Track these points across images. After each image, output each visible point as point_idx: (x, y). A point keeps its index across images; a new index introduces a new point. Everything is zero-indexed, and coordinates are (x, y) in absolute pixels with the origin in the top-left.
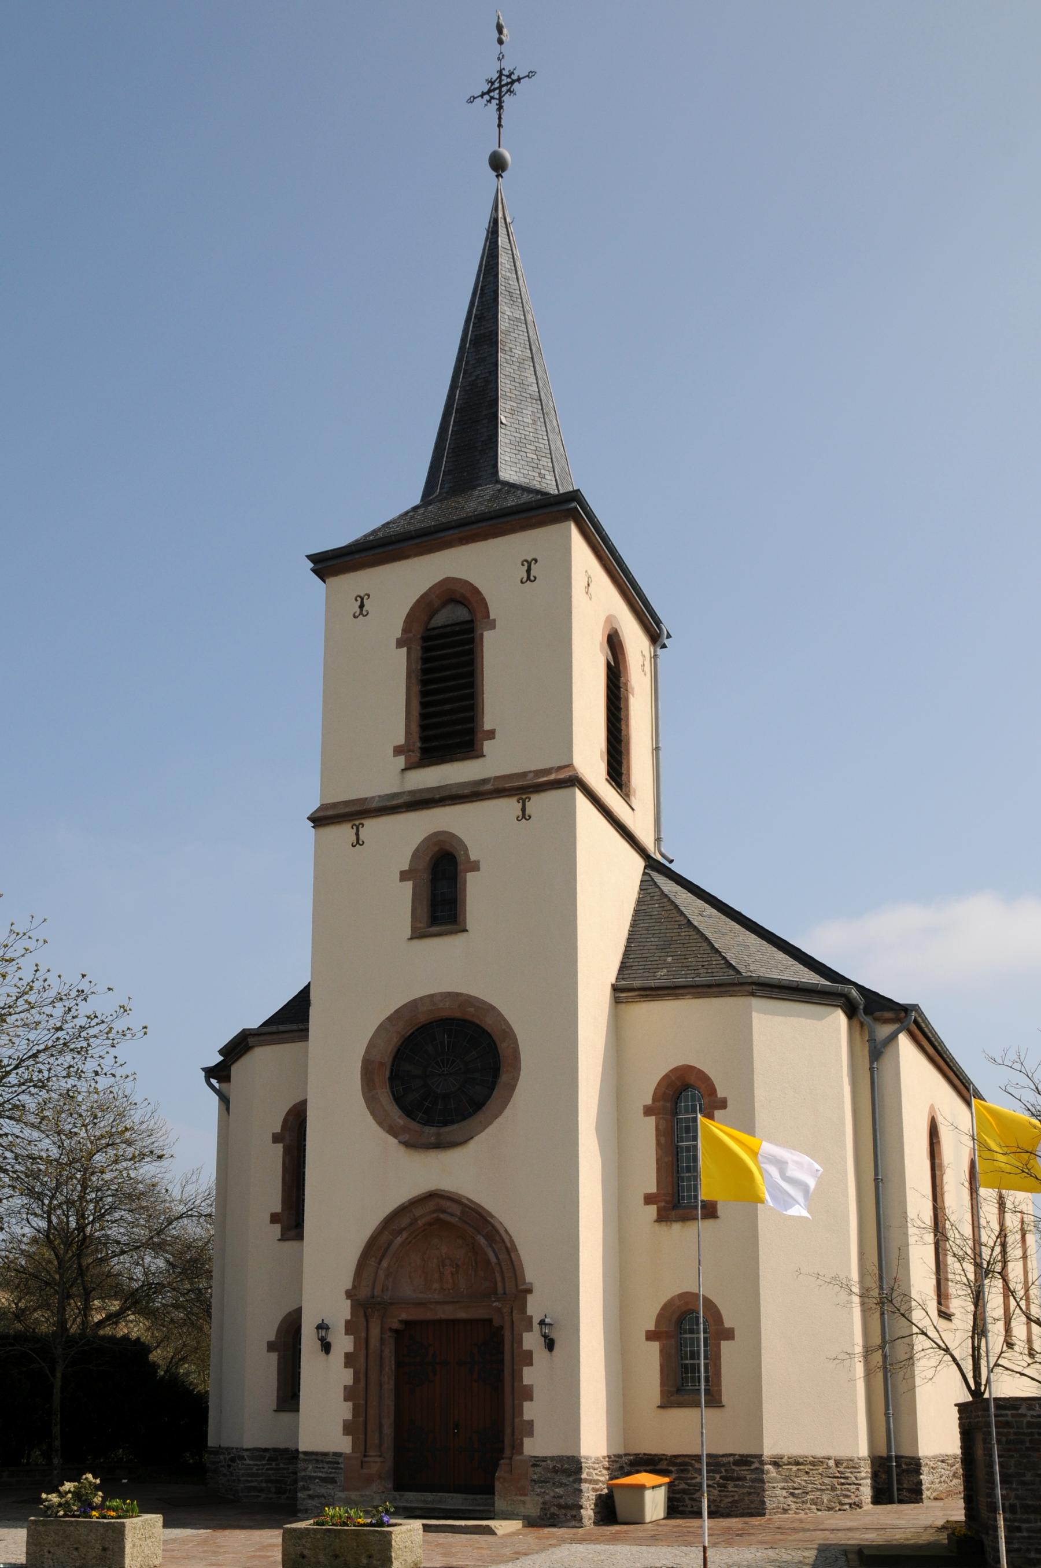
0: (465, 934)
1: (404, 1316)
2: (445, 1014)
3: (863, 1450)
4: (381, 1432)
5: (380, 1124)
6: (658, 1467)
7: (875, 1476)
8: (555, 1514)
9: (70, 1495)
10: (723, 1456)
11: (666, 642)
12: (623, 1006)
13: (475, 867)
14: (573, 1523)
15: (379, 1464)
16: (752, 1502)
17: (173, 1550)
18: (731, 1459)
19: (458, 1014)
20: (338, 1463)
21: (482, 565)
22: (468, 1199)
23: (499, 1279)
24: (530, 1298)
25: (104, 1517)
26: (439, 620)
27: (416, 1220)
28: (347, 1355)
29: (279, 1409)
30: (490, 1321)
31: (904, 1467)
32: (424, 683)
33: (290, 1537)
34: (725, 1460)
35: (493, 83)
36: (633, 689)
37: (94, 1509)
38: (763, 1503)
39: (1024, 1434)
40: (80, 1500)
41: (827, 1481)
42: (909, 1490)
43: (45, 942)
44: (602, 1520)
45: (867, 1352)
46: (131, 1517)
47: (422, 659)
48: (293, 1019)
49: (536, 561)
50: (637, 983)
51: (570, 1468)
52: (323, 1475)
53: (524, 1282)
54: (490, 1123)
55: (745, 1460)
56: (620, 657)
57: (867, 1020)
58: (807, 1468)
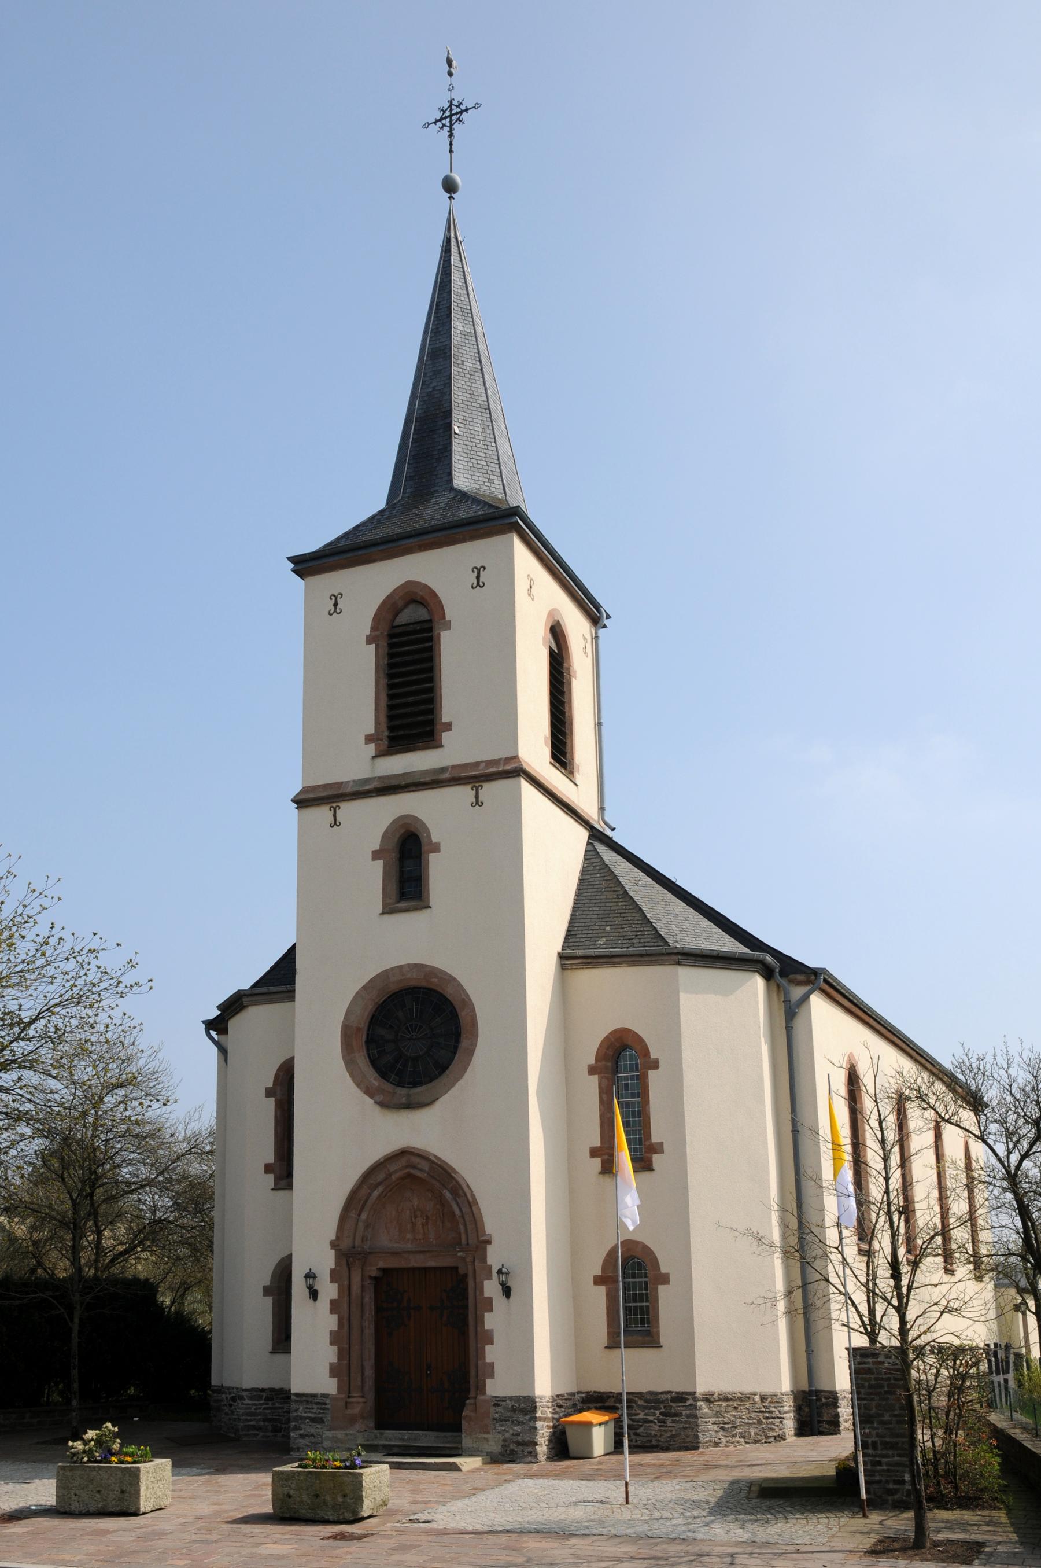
0: (429, 910)
1: (381, 1264)
2: (413, 983)
3: (785, 1385)
4: (363, 1374)
5: (358, 1085)
6: (606, 1404)
7: (798, 1409)
8: (513, 1452)
9: (93, 1443)
10: (662, 1393)
11: (606, 622)
12: (569, 972)
13: (436, 848)
14: (530, 1459)
15: (362, 1404)
16: (688, 1436)
17: (181, 1490)
18: (669, 1396)
19: (424, 984)
20: (325, 1404)
21: (440, 570)
22: (435, 1156)
23: (462, 1230)
24: (490, 1249)
25: (122, 1462)
26: (404, 618)
27: (390, 1175)
28: (332, 1302)
29: (274, 1352)
30: (457, 1268)
31: (824, 1400)
32: (390, 676)
33: (278, 1478)
34: (664, 1397)
35: (444, 112)
36: (575, 672)
37: (113, 1455)
38: (697, 1437)
39: (882, 1379)
40: (101, 1446)
41: (753, 1415)
42: (829, 1423)
43: (59, 899)
44: (557, 1455)
45: (789, 1293)
46: (145, 1462)
47: (388, 654)
48: (280, 980)
49: (484, 568)
50: (580, 952)
51: (527, 1406)
52: (312, 1415)
53: (484, 1234)
54: (453, 1085)
55: (680, 1397)
56: (562, 642)
57: (783, 982)
58: (735, 1404)
